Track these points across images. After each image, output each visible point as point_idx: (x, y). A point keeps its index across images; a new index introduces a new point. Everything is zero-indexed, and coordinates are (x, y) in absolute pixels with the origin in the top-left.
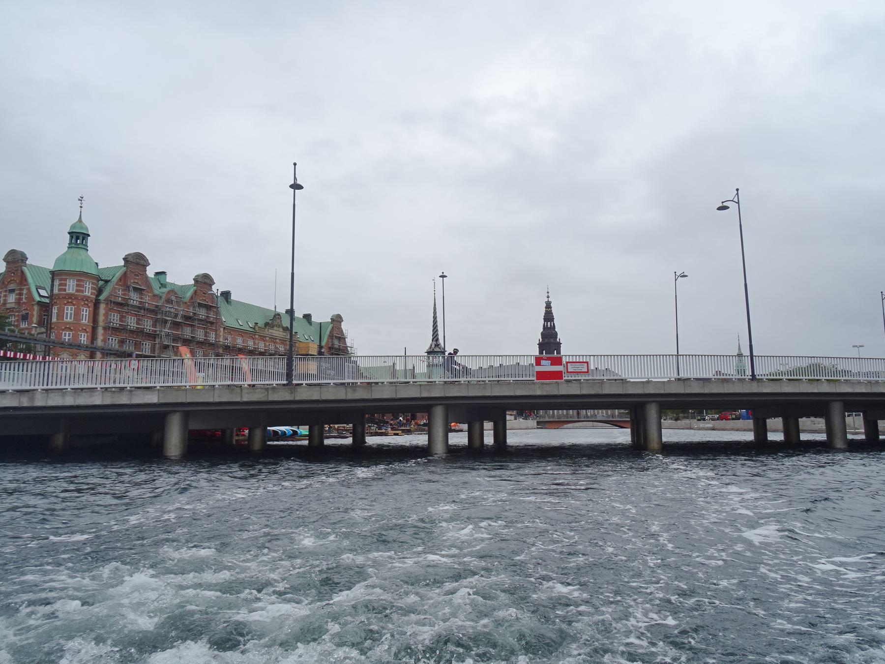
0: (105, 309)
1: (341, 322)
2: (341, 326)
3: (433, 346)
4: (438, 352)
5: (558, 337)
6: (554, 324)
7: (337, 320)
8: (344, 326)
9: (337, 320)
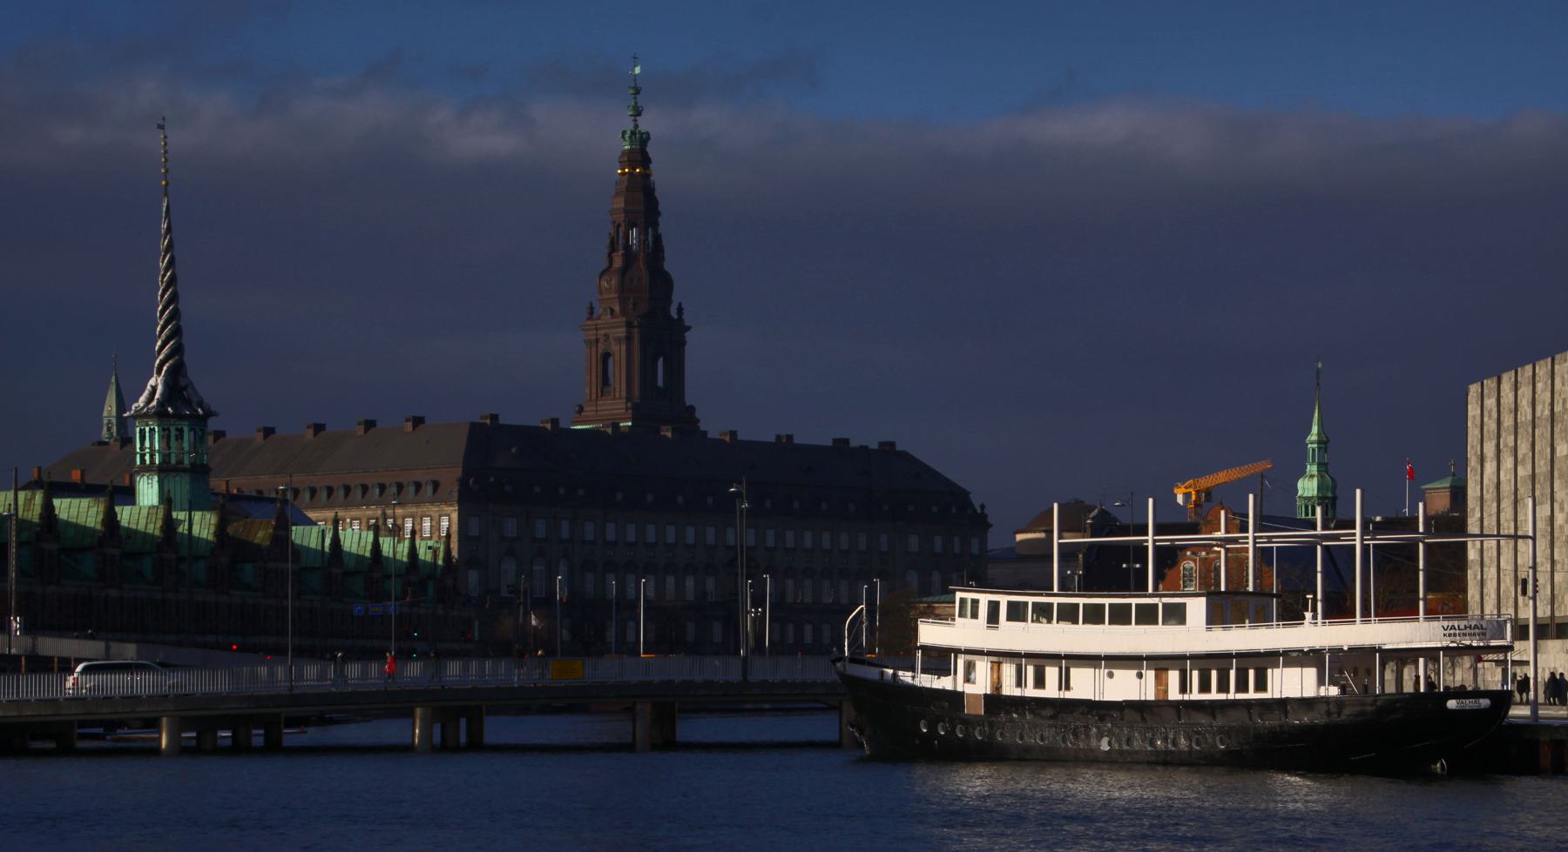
5: (676, 298)
6: (658, 239)
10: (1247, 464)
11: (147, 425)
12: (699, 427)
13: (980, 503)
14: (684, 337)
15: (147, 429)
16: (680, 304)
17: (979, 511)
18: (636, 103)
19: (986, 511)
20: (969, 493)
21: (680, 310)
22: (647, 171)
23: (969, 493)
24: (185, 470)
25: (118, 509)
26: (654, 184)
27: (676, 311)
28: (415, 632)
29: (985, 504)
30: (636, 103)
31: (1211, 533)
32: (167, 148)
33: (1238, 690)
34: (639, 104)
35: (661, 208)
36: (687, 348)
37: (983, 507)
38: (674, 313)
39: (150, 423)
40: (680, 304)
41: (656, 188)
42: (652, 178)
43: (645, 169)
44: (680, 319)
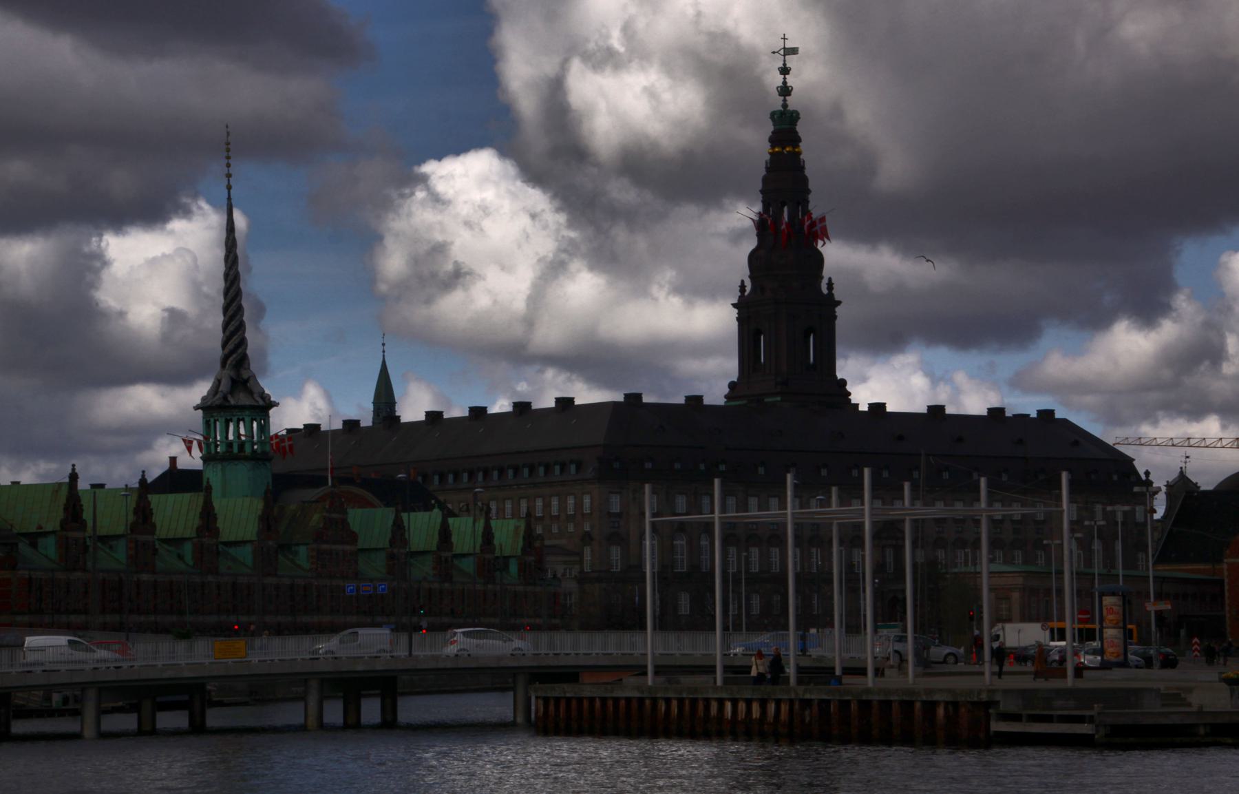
3: (224, 386)
4: (242, 408)
5: (826, 273)
10: (496, 640)
11: (212, 417)
12: (850, 400)
13: (1144, 470)
14: (835, 312)
15: (212, 420)
16: (830, 279)
17: (1143, 477)
18: (785, 64)
19: (1151, 478)
20: (1134, 460)
21: (830, 285)
22: (797, 150)
23: (1134, 460)
24: (246, 459)
25: (150, 497)
26: (804, 161)
27: (826, 286)
28: (421, 610)
29: (1149, 470)
30: (785, 64)
31: (658, 591)
32: (226, 154)
33: (681, 569)
34: (787, 66)
35: (811, 186)
36: (837, 322)
37: (1147, 473)
38: (825, 290)
39: (215, 414)
40: (830, 279)
41: (806, 166)
42: (802, 157)
43: (794, 148)
44: (831, 295)
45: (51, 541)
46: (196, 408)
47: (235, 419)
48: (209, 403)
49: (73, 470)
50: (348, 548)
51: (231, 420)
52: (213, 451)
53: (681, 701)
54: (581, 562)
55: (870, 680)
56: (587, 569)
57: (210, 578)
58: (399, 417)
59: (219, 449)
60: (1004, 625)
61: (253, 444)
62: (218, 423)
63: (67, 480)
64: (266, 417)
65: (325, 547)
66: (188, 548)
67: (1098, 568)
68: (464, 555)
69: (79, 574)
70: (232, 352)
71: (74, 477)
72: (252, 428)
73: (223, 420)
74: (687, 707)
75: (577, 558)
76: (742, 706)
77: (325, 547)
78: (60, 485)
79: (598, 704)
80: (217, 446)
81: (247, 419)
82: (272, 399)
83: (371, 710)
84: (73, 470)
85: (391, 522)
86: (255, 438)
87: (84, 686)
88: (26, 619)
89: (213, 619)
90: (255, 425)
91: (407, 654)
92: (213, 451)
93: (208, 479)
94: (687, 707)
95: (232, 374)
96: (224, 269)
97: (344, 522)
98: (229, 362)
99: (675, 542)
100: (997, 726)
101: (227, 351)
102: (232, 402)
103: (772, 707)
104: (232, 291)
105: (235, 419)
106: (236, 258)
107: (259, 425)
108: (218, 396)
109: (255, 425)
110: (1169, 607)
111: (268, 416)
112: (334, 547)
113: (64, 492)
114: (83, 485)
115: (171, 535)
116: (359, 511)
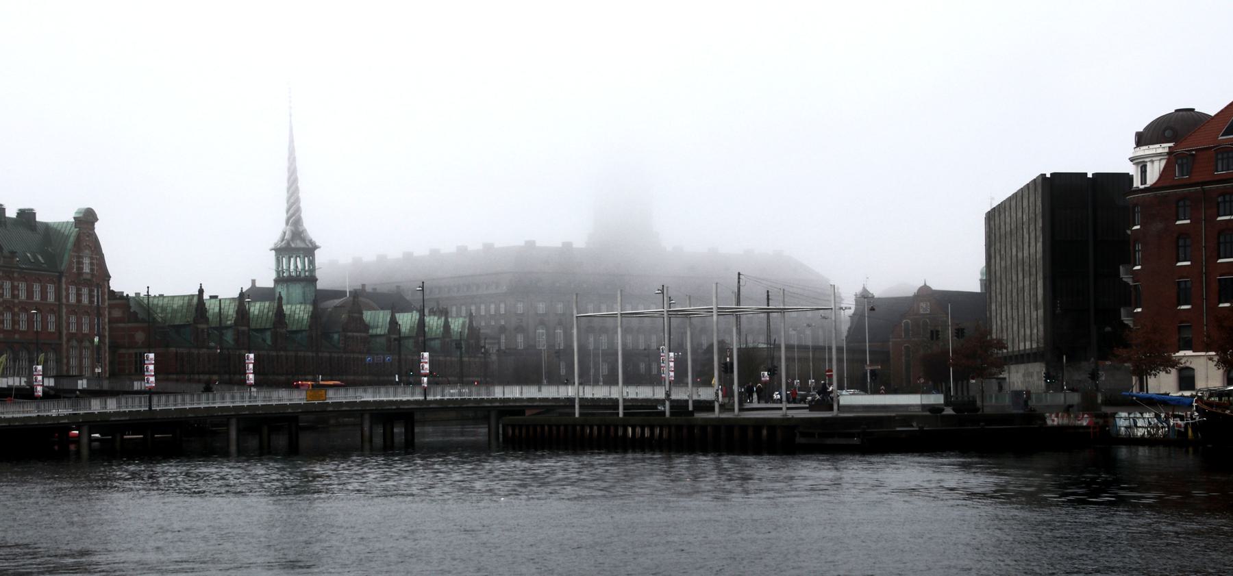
0: (66, 284)
1: (93, 224)
2: (94, 229)
7: (87, 220)
8: (99, 229)
9: (87, 220)
11: (281, 254)
45: (411, 341)
46: (271, 250)
47: (294, 256)
48: (279, 246)
49: (201, 287)
50: (363, 334)
51: (292, 257)
52: (281, 276)
53: (550, 427)
54: (499, 343)
55: (716, 414)
56: (503, 347)
57: (282, 353)
58: (127, 295)
59: (285, 275)
60: (520, 397)
61: (305, 271)
62: (284, 259)
63: (197, 293)
64: (313, 255)
65: (350, 334)
66: (268, 335)
67: (30, 412)
68: (434, 339)
69: (204, 350)
70: (293, 215)
71: (201, 291)
72: (304, 262)
73: (287, 257)
74: (603, 431)
75: (496, 341)
76: (638, 430)
77: (350, 334)
78: (193, 296)
79: (562, 428)
80: (283, 273)
81: (301, 256)
82: (317, 244)
83: (281, 441)
84: (201, 287)
85: (388, 319)
86: (307, 268)
87: (229, 418)
88: (175, 377)
89: (283, 378)
90: (306, 259)
91: (423, 398)
92: (281, 276)
93: (280, 293)
94: (603, 431)
95: (293, 228)
96: (96, 231)
97: (361, 319)
98: (290, 221)
99: (556, 331)
100: (800, 440)
101: (289, 214)
102: (293, 245)
103: (657, 431)
104: (292, 178)
105: (294, 256)
106: (294, 158)
107: (309, 260)
108: (284, 242)
109: (306, 259)
110: (879, 367)
111: (314, 254)
112: (355, 334)
113: (195, 300)
114: (206, 296)
115: (258, 327)
116: (369, 313)
